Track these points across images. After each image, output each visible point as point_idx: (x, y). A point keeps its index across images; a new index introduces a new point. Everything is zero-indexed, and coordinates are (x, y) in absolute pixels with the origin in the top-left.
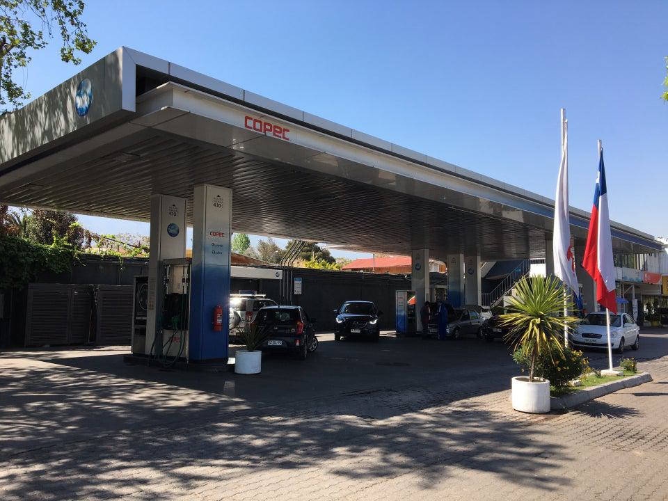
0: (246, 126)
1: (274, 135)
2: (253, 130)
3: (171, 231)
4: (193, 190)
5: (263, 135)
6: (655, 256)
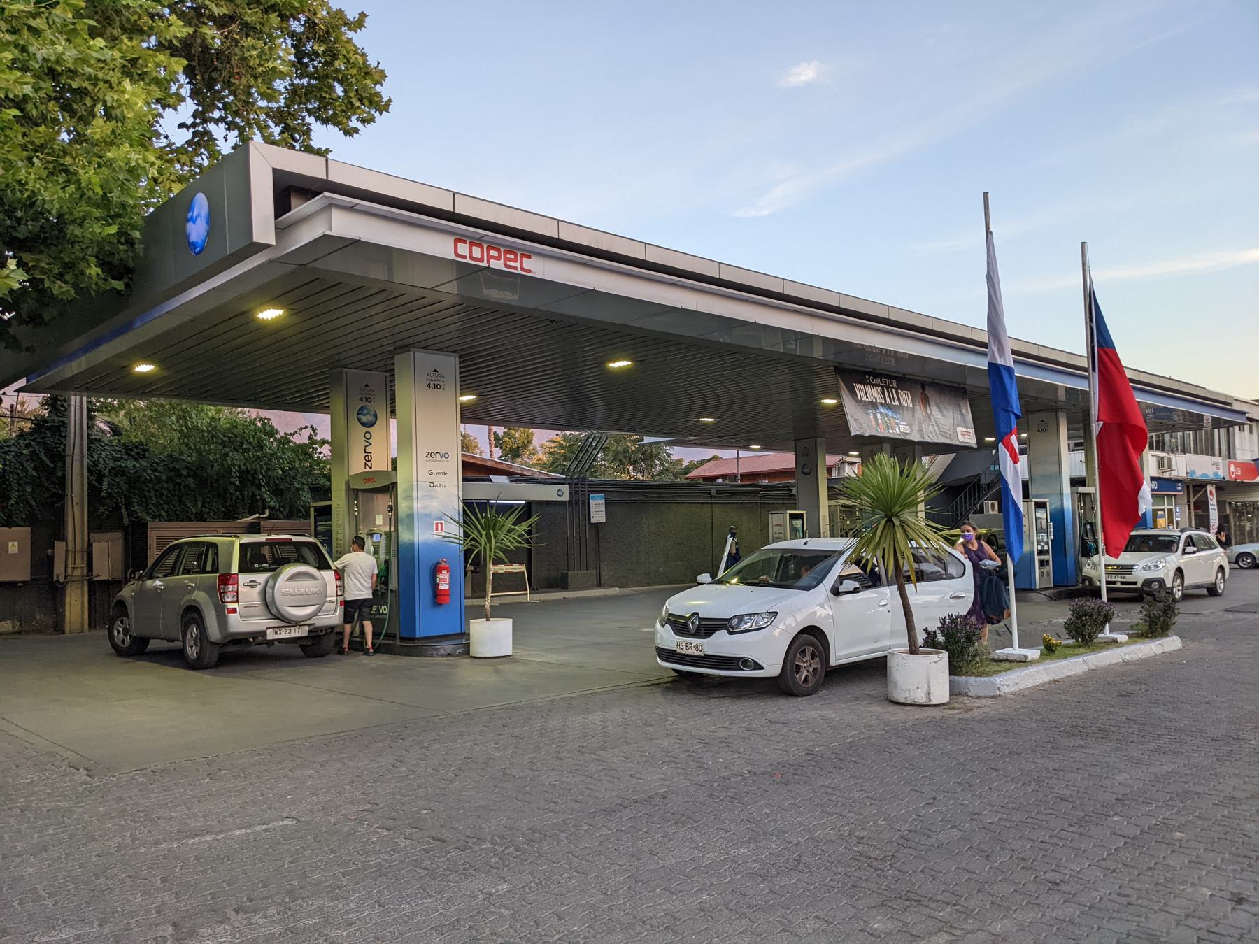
0: (457, 254)
1: (506, 265)
2: (468, 261)
3: (364, 419)
4: (393, 358)
5: (485, 268)
6: (1251, 432)
